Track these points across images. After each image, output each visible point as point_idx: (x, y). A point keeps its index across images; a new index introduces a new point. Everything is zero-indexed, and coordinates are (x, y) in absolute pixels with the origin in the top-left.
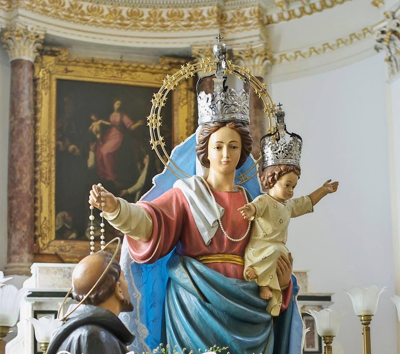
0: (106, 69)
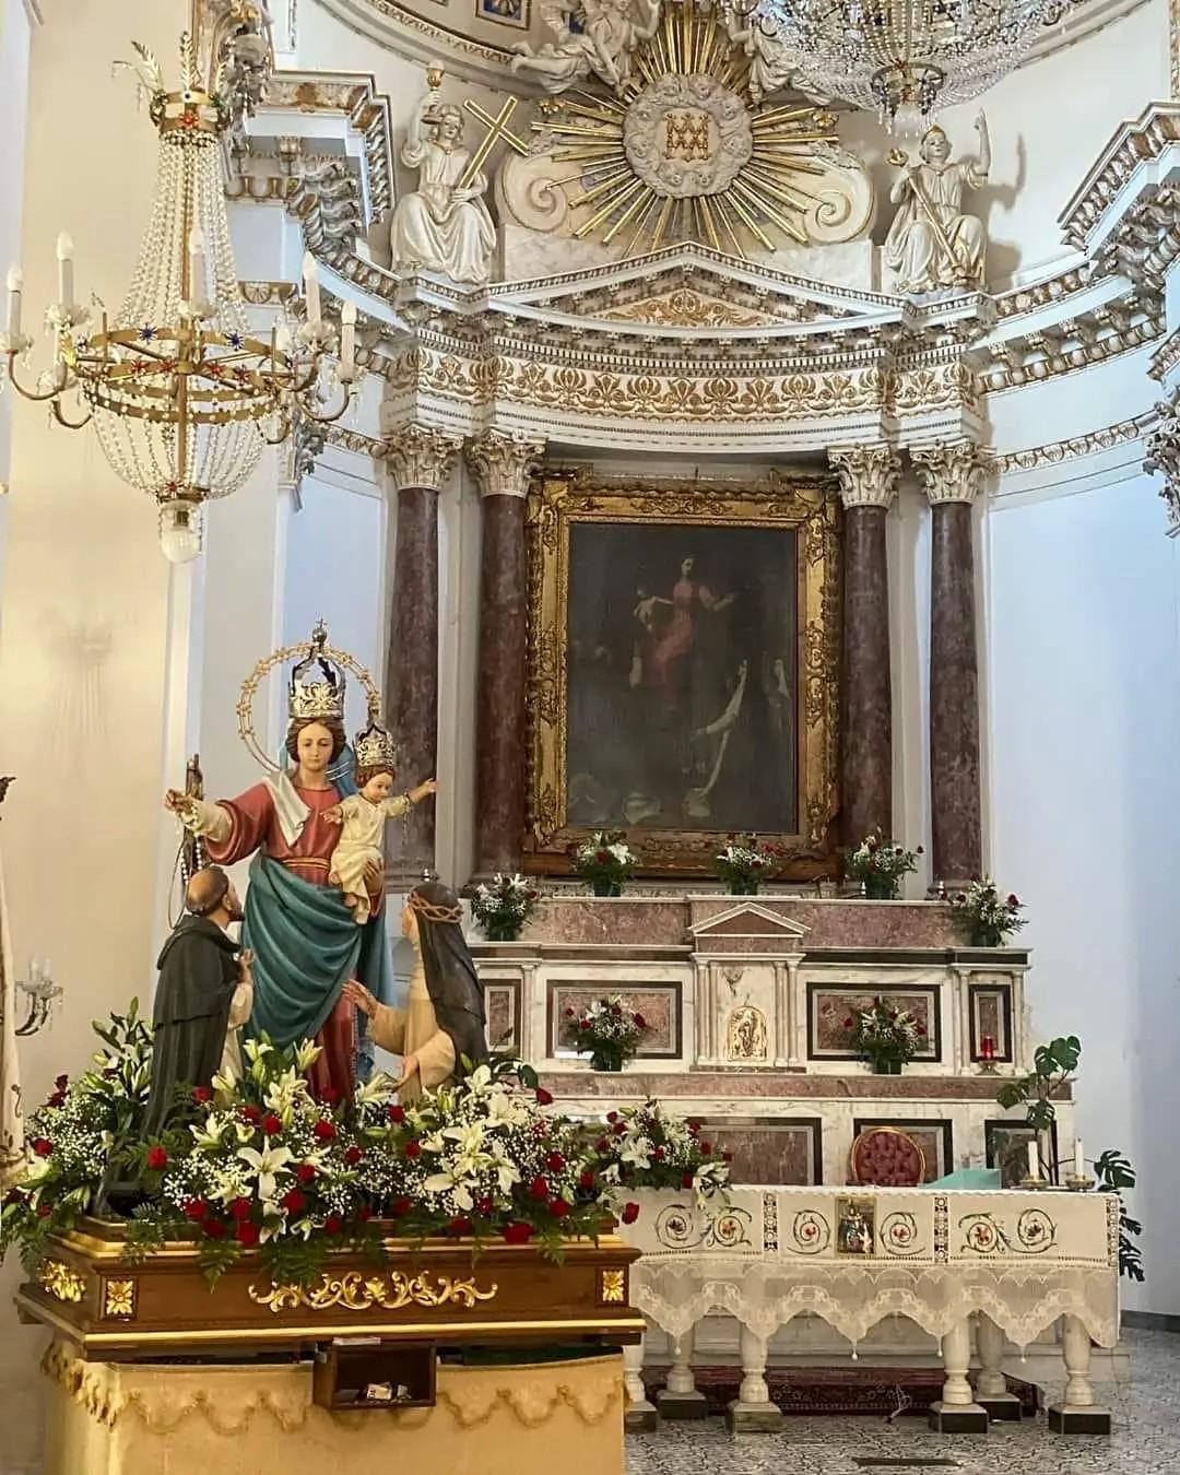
0: (664, 500)
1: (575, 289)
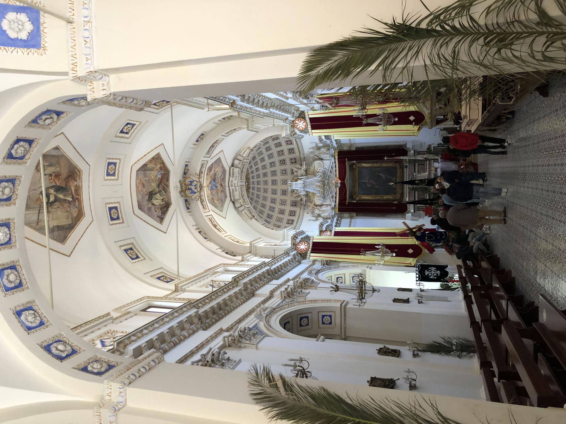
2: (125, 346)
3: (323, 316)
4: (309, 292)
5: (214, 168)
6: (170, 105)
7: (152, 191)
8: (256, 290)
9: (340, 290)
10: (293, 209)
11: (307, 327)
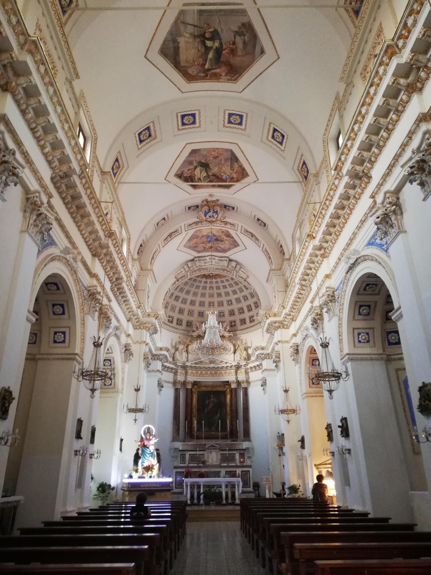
1: (197, 361)
2: (30, 52)
3: (64, 333)
4: (94, 320)
5: (229, 240)
6: (302, 180)
7: (209, 167)
8: (100, 260)
9: (96, 348)
10: (184, 323)
11: (51, 313)
